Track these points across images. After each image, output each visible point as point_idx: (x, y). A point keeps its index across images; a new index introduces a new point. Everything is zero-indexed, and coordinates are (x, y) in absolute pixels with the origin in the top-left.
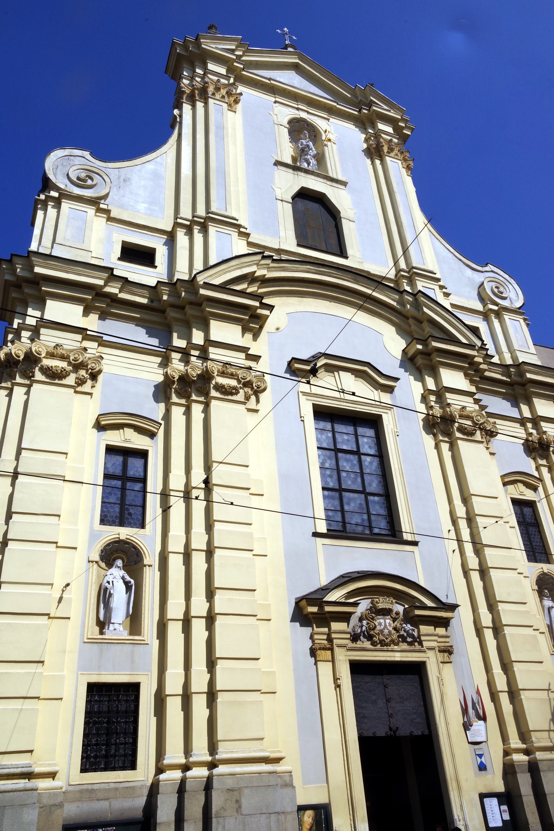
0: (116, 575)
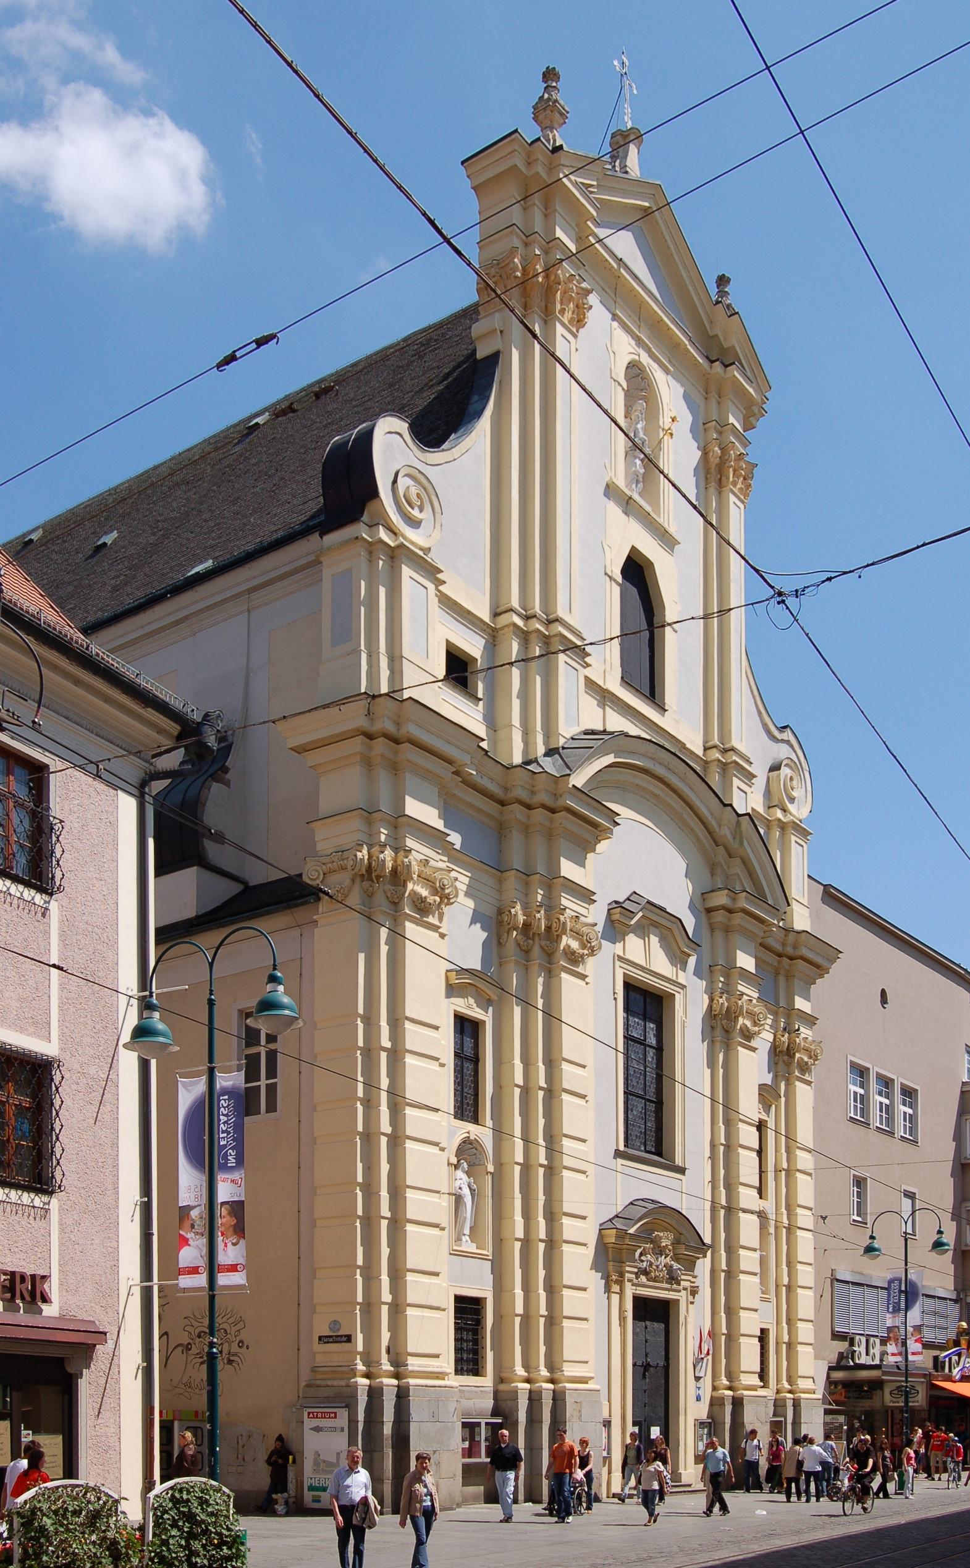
0: (462, 1179)
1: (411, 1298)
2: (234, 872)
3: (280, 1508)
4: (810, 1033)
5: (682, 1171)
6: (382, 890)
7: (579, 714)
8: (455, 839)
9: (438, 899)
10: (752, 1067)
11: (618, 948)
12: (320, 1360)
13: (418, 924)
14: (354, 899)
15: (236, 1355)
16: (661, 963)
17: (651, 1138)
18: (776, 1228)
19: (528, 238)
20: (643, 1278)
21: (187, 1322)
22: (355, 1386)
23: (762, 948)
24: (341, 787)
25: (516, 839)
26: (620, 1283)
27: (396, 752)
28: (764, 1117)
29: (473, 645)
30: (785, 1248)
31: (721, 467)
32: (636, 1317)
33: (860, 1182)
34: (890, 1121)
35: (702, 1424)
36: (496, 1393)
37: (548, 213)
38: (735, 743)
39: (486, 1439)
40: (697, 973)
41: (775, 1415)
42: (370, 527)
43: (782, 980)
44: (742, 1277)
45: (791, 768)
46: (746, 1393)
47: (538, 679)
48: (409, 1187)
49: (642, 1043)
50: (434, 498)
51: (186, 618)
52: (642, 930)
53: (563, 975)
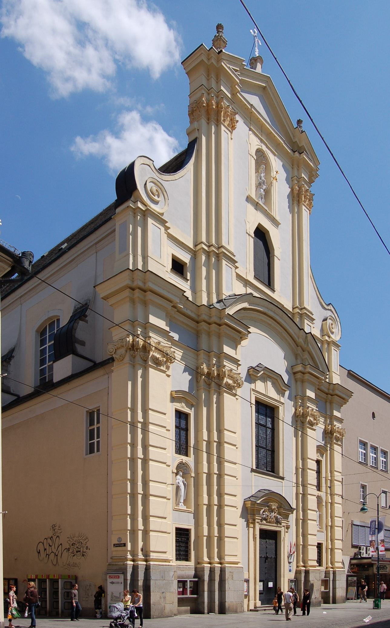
0: (180, 479)
1: (152, 527)
2: (90, 358)
3: (98, 615)
4: (340, 425)
5: (283, 478)
6: (139, 354)
7: (232, 287)
8: (176, 337)
9: (165, 359)
10: (315, 436)
11: (253, 386)
12: (114, 554)
13: (155, 370)
14: (127, 358)
15: (85, 552)
16: (272, 393)
17: (269, 464)
18: (326, 503)
19: (209, 90)
20: (264, 522)
21: (68, 539)
22: (126, 565)
23: (318, 390)
24: (122, 312)
25: (204, 339)
26: (254, 523)
27: (145, 296)
28: (320, 458)
29: (185, 257)
30: (330, 511)
31: (299, 195)
32: (261, 537)
33: (364, 487)
34: (376, 463)
35: (291, 581)
36: (196, 569)
37: (218, 82)
38: (306, 305)
39: (190, 587)
40: (290, 398)
41: (325, 577)
42: (135, 203)
43: (328, 404)
44: (309, 521)
45: (332, 320)
46: (310, 568)
47: (214, 271)
48: (151, 481)
49: (265, 426)
50: (165, 193)
51: (74, 259)
52: (264, 379)
53: (225, 394)
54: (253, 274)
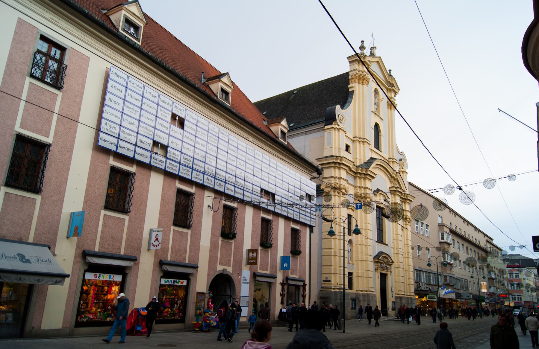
29: (350, 144)
54: (374, 146)
